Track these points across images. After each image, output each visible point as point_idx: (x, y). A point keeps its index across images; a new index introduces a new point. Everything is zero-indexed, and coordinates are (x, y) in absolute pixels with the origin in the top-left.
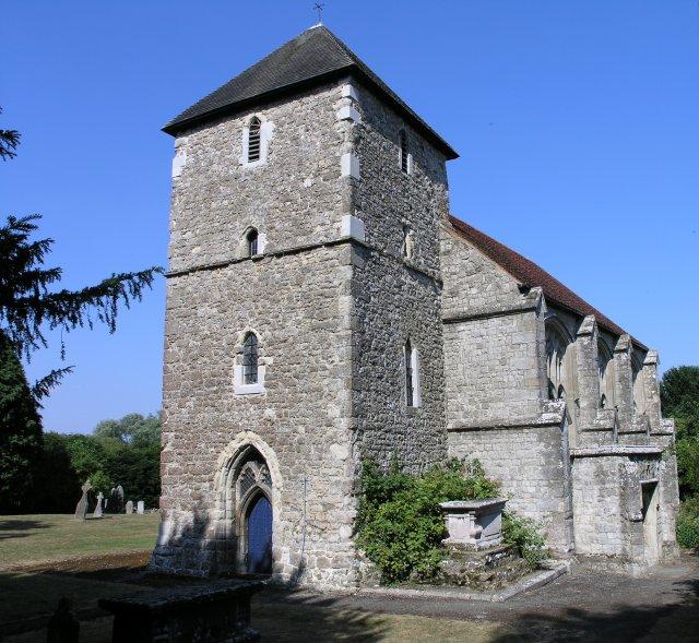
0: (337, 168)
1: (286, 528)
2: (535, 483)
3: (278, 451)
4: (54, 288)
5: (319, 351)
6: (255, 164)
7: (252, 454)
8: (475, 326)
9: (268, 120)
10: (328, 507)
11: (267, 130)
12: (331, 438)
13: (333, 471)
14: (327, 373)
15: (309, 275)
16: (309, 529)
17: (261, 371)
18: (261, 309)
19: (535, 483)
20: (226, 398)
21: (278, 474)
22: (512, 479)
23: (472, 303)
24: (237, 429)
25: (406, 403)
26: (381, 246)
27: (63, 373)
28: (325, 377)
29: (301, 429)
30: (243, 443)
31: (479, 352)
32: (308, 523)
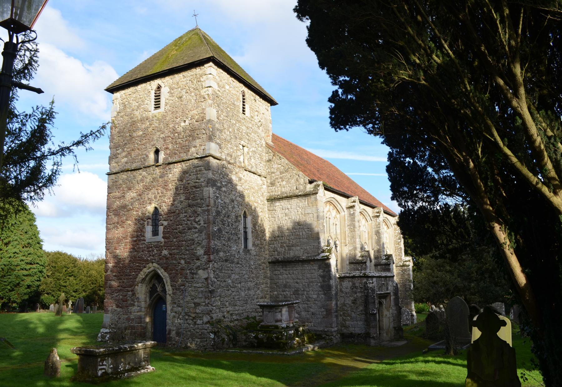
0: (203, 115)
1: (174, 317)
2: (316, 293)
3: (170, 274)
4: (26, 9)
5: (193, 218)
6: (158, 111)
7: (156, 277)
8: (284, 203)
9: (166, 83)
10: (197, 305)
11: (165, 91)
12: (199, 266)
13: (200, 285)
14: (197, 230)
15: (187, 175)
16: (187, 317)
17: (161, 229)
18: (161, 194)
19: (316, 293)
20: (142, 244)
21: (170, 287)
22: (304, 291)
23: (283, 190)
24: (147, 262)
25: (243, 247)
26: (229, 159)
27: (74, 148)
28: (196, 233)
29: (183, 262)
30: (150, 270)
31: (287, 218)
32: (186, 314)
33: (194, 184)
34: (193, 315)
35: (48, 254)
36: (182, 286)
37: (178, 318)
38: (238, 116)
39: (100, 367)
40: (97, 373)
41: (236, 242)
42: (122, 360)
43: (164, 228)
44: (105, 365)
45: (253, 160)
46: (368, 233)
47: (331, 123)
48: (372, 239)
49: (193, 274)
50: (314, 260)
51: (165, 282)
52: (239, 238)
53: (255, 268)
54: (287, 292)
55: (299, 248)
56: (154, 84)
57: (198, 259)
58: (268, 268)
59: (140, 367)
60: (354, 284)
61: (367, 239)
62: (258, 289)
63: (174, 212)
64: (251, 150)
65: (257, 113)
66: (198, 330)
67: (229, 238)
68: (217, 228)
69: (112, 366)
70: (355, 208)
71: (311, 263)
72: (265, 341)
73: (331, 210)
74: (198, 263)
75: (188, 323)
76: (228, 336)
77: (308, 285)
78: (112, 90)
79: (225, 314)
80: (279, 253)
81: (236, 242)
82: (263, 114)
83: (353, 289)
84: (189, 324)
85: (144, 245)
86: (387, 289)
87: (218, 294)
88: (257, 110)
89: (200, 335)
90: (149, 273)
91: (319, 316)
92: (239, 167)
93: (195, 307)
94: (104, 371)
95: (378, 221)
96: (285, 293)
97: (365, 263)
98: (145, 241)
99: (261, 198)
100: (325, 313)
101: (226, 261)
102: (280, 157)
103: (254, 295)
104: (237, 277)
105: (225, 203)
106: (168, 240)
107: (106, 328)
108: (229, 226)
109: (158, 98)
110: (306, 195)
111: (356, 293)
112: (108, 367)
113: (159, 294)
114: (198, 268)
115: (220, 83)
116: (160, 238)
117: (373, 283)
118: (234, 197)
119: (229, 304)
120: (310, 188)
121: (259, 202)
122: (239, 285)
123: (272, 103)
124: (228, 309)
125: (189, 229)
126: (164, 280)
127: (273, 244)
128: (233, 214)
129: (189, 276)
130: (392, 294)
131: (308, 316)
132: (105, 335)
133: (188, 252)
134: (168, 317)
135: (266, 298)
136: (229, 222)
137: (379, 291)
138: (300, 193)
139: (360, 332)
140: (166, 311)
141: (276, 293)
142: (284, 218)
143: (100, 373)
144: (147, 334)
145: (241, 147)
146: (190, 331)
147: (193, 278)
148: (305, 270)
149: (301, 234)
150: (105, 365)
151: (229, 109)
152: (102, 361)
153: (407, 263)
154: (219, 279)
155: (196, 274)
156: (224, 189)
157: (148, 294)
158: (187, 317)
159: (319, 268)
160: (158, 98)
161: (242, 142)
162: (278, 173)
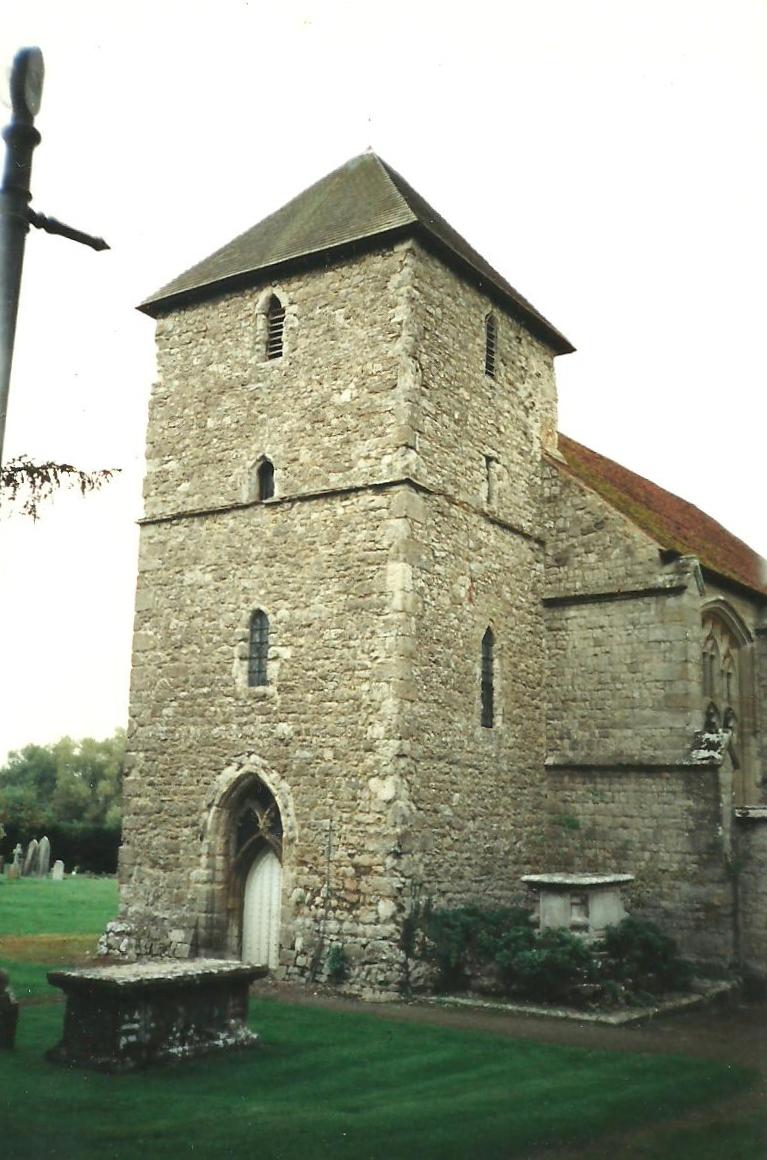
10: (362, 871)
13: (370, 818)
17: (273, 669)
22: (643, 849)
31: (597, 650)
33: (362, 554)
34: (354, 898)
37: (312, 902)
39: (125, 1027)
42: (181, 1009)
49: (356, 787)
51: (281, 807)
53: (512, 781)
55: (629, 732)
57: (369, 750)
58: (545, 783)
63: (309, 626)
71: (667, 775)
78: (155, 308)
82: (538, 375)
90: (240, 779)
91: (683, 923)
99: (530, 595)
102: (582, 490)
114: (369, 773)
120: (663, 578)
123: (98, 245)
124: (443, 887)
144: (229, 940)
147: (354, 799)
148: (646, 792)
157: (233, 837)
158: (334, 902)
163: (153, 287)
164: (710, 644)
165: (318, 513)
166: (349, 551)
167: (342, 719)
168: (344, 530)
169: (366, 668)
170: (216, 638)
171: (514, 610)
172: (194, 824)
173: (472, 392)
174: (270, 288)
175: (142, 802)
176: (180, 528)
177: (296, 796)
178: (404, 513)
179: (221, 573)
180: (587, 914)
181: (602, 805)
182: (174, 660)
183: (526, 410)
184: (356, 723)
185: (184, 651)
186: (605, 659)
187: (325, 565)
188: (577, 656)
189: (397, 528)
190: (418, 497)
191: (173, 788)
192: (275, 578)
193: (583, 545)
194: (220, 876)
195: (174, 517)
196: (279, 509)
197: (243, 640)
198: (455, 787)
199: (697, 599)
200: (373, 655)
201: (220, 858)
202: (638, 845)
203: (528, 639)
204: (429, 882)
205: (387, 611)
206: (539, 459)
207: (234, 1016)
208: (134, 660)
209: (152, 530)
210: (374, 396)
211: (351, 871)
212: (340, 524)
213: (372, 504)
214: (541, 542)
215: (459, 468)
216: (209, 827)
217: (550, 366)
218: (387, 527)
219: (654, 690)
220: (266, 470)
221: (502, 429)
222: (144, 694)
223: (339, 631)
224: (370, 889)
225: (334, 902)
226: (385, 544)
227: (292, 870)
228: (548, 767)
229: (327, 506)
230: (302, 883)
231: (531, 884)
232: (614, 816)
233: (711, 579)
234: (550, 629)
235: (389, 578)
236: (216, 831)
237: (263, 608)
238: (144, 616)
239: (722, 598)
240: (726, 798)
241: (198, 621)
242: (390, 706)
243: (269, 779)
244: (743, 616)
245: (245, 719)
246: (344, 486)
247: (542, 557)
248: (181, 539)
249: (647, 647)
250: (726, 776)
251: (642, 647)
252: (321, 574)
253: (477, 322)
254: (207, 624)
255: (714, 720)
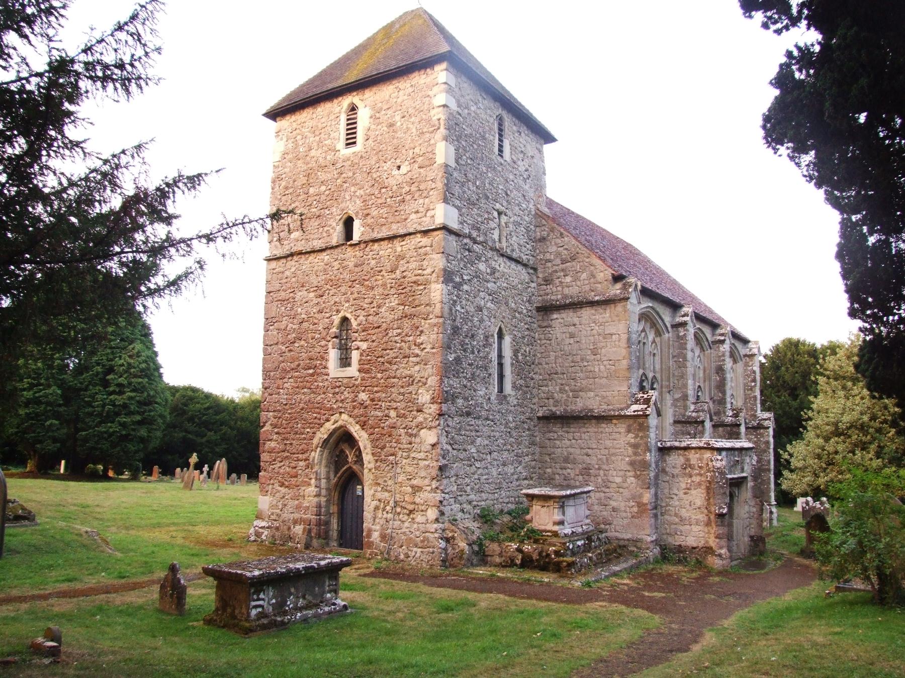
2: (622, 473)
5: (411, 338)
7: (344, 438)
9: (366, 103)
10: (416, 489)
11: (363, 118)
13: (422, 455)
17: (355, 356)
19: (622, 473)
20: (323, 381)
22: (599, 469)
25: (496, 390)
29: (393, 414)
31: (572, 341)
33: (414, 278)
34: (411, 507)
35: (174, 390)
36: (392, 455)
37: (384, 510)
38: (490, 159)
40: (249, 614)
41: (485, 381)
42: (293, 590)
43: (361, 355)
44: (263, 600)
45: (514, 238)
46: (705, 371)
47: (765, 138)
48: (710, 380)
49: (411, 435)
50: (620, 417)
51: (362, 448)
52: (490, 375)
53: (516, 428)
54: (569, 470)
55: (592, 394)
56: (346, 101)
57: (419, 411)
59: (322, 602)
60: (688, 460)
61: (702, 381)
62: (520, 463)
63: (379, 327)
64: (512, 220)
65: (522, 155)
66: (418, 533)
67: (473, 374)
68: (453, 355)
69: (274, 601)
70: (688, 327)
71: (614, 421)
72: (535, 556)
73: (648, 330)
74: (420, 418)
75: (400, 520)
76: (469, 545)
77: (607, 459)
78: (275, 114)
79: (465, 506)
80: (557, 401)
81: (485, 381)
82: (532, 157)
83: (685, 468)
84: (403, 522)
85: (326, 384)
86: (742, 470)
87: (452, 473)
88: (523, 149)
89: (422, 541)
90: (335, 430)
91: (624, 514)
92: (491, 249)
93: (414, 494)
94: (260, 610)
95: (721, 349)
96: (564, 472)
97: (703, 422)
98: (328, 375)
100: (635, 509)
101: (468, 414)
102: (561, 234)
103: (512, 474)
104: (486, 442)
105: (467, 312)
106: (368, 375)
107: (263, 520)
108: (473, 353)
109: (352, 126)
110: (608, 302)
111: (691, 476)
112: (268, 602)
113: (350, 468)
114: (420, 427)
115: (462, 100)
116: (353, 371)
117: (721, 460)
118: (482, 303)
119: (472, 489)
120: (616, 290)
121: (525, 311)
122: (488, 457)
125: (405, 357)
126: (360, 444)
127: (547, 386)
128: (480, 331)
129: (405, 439)
130: (749, 479)
131: (605, 513)
132: (261, 530)
133: (402, 397)
134: (366, 507)
135: (532, 478)
136: (473, 347)
137: (730, 473)
138: (597, 298)
139: (695, 545)
140: (363, 497)
141: (549, 470)
142: (568, 341)
143: (254, 612)
144: (331, 533)
145: (496, 214)
146: (404, 533)
147: (410, 443)
148: (602, 432)
149: (597, 370)
150: (263, 600)
151: (475, 147)
152: (258, 592)
153: (766, 423)
154: (455, 446)
155: (415, 436)
156: (465, 287)
157: (332, 467)
158: (398, 510)
159: (629, 431)
160: (352, 126)
161: (498, 206)
162: (558, 261)
163: (275, 97)
164: (643, 334)
165: (384, 249)
166: (404, 277)
167: (402, 390)
168: (402, 262)
169: (417, 356)
170: (317, 336)
171: (517, 314)
172: (306, 460)
173: (488, 167)
174: (350, 97)
175: (273, 444)
176: (293, 263)
177: (372, 441)
178: (442, 250)
179: (320, 293)
180: (564, 514)
181: (573, 441)
182: (290, 351)
183: (525, 180)
184: (411, 393)
185: (296, 345)
186: (576, 346)
187: (389, 286)
188: (558, 344)
189: (438, 262)
190: (452, 238)
191: (292, 436)
192: (356, 295)
193: (563, 270)
194: (324, 492)
195: (288, 256)
196: (357, 248)
197: (336, 337)
198: (478, 434)
199: (636, 305)
200: (422, 347)
201: (324, 481)
202: (597, 466)
203: (526, 333)
204: (461, 496)
205: (431, 317)
206: (533, 213)
207: (330, 592)
208: (265, 350)
209: (274, 264)
210: (421, 170)
211: (409, 489)
212: (400, 257)
213: (421, 244)
214: (535, 269)
215: (479, 219)
216: (316, 461)
217: (540, 151)
218: (431, 259)
219: (608, 367)
220: (348, 223)
221: (509, 192)
222: (272, 374)
223: (399, 331)
224: (422, 502)
225: (398, 510)
226: (429, 271)
227: (370, 489)
228: (539, 418)
229: (390, 245)
230: (377, 497)
231: (527, 495)
232: (581, 448)
233: (646, 293)
234: (540, 326)
235: (432, 294)
236: (321, 462)
237: (349, 316)
238: (270, 321)
239: (651, 305)
240: (652, 435)
241: (305, 325)
242: (433, 381)
243: (355, 430)
244: (663, 317)
245: (337, 390)
246: (402, 231)
247: (535, 278)
248: (293, 269)
249: (604, 338)
250: (653, 421)
251: (601, 338)
252: (386, 292)
253: (492, 120)
254: (311, 327)
255: (644, 384)
